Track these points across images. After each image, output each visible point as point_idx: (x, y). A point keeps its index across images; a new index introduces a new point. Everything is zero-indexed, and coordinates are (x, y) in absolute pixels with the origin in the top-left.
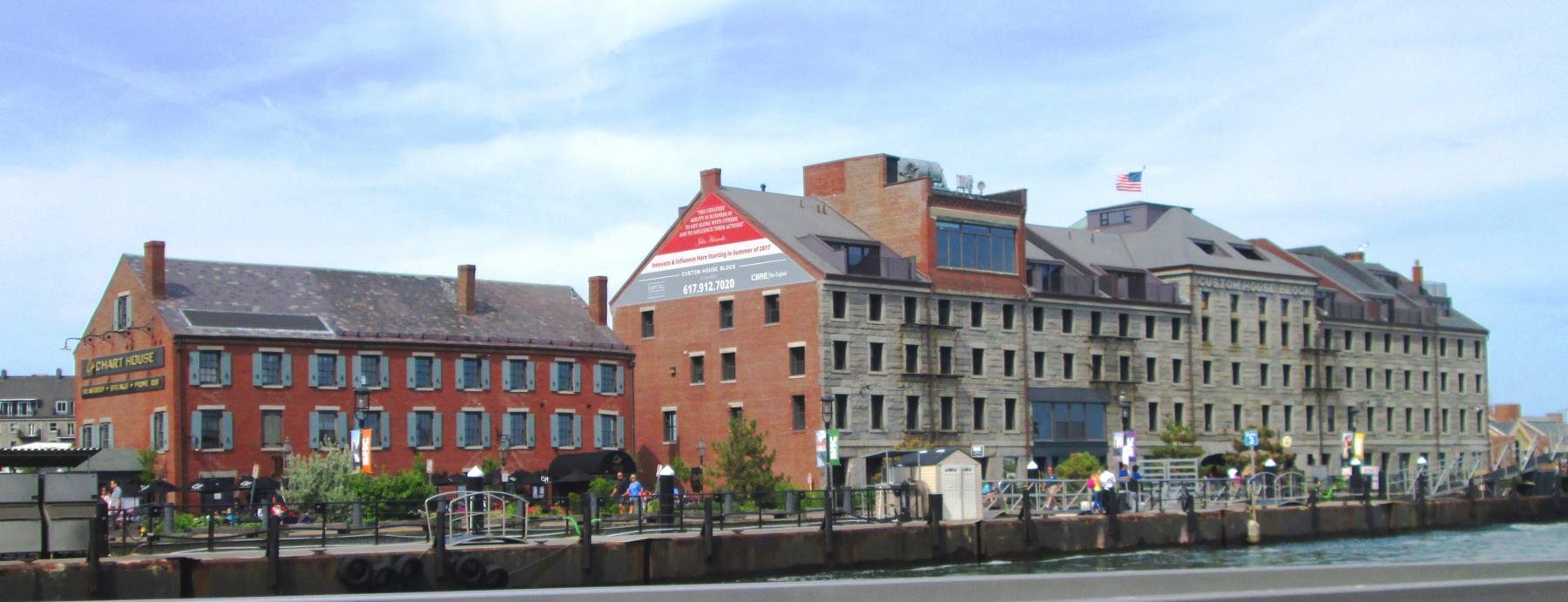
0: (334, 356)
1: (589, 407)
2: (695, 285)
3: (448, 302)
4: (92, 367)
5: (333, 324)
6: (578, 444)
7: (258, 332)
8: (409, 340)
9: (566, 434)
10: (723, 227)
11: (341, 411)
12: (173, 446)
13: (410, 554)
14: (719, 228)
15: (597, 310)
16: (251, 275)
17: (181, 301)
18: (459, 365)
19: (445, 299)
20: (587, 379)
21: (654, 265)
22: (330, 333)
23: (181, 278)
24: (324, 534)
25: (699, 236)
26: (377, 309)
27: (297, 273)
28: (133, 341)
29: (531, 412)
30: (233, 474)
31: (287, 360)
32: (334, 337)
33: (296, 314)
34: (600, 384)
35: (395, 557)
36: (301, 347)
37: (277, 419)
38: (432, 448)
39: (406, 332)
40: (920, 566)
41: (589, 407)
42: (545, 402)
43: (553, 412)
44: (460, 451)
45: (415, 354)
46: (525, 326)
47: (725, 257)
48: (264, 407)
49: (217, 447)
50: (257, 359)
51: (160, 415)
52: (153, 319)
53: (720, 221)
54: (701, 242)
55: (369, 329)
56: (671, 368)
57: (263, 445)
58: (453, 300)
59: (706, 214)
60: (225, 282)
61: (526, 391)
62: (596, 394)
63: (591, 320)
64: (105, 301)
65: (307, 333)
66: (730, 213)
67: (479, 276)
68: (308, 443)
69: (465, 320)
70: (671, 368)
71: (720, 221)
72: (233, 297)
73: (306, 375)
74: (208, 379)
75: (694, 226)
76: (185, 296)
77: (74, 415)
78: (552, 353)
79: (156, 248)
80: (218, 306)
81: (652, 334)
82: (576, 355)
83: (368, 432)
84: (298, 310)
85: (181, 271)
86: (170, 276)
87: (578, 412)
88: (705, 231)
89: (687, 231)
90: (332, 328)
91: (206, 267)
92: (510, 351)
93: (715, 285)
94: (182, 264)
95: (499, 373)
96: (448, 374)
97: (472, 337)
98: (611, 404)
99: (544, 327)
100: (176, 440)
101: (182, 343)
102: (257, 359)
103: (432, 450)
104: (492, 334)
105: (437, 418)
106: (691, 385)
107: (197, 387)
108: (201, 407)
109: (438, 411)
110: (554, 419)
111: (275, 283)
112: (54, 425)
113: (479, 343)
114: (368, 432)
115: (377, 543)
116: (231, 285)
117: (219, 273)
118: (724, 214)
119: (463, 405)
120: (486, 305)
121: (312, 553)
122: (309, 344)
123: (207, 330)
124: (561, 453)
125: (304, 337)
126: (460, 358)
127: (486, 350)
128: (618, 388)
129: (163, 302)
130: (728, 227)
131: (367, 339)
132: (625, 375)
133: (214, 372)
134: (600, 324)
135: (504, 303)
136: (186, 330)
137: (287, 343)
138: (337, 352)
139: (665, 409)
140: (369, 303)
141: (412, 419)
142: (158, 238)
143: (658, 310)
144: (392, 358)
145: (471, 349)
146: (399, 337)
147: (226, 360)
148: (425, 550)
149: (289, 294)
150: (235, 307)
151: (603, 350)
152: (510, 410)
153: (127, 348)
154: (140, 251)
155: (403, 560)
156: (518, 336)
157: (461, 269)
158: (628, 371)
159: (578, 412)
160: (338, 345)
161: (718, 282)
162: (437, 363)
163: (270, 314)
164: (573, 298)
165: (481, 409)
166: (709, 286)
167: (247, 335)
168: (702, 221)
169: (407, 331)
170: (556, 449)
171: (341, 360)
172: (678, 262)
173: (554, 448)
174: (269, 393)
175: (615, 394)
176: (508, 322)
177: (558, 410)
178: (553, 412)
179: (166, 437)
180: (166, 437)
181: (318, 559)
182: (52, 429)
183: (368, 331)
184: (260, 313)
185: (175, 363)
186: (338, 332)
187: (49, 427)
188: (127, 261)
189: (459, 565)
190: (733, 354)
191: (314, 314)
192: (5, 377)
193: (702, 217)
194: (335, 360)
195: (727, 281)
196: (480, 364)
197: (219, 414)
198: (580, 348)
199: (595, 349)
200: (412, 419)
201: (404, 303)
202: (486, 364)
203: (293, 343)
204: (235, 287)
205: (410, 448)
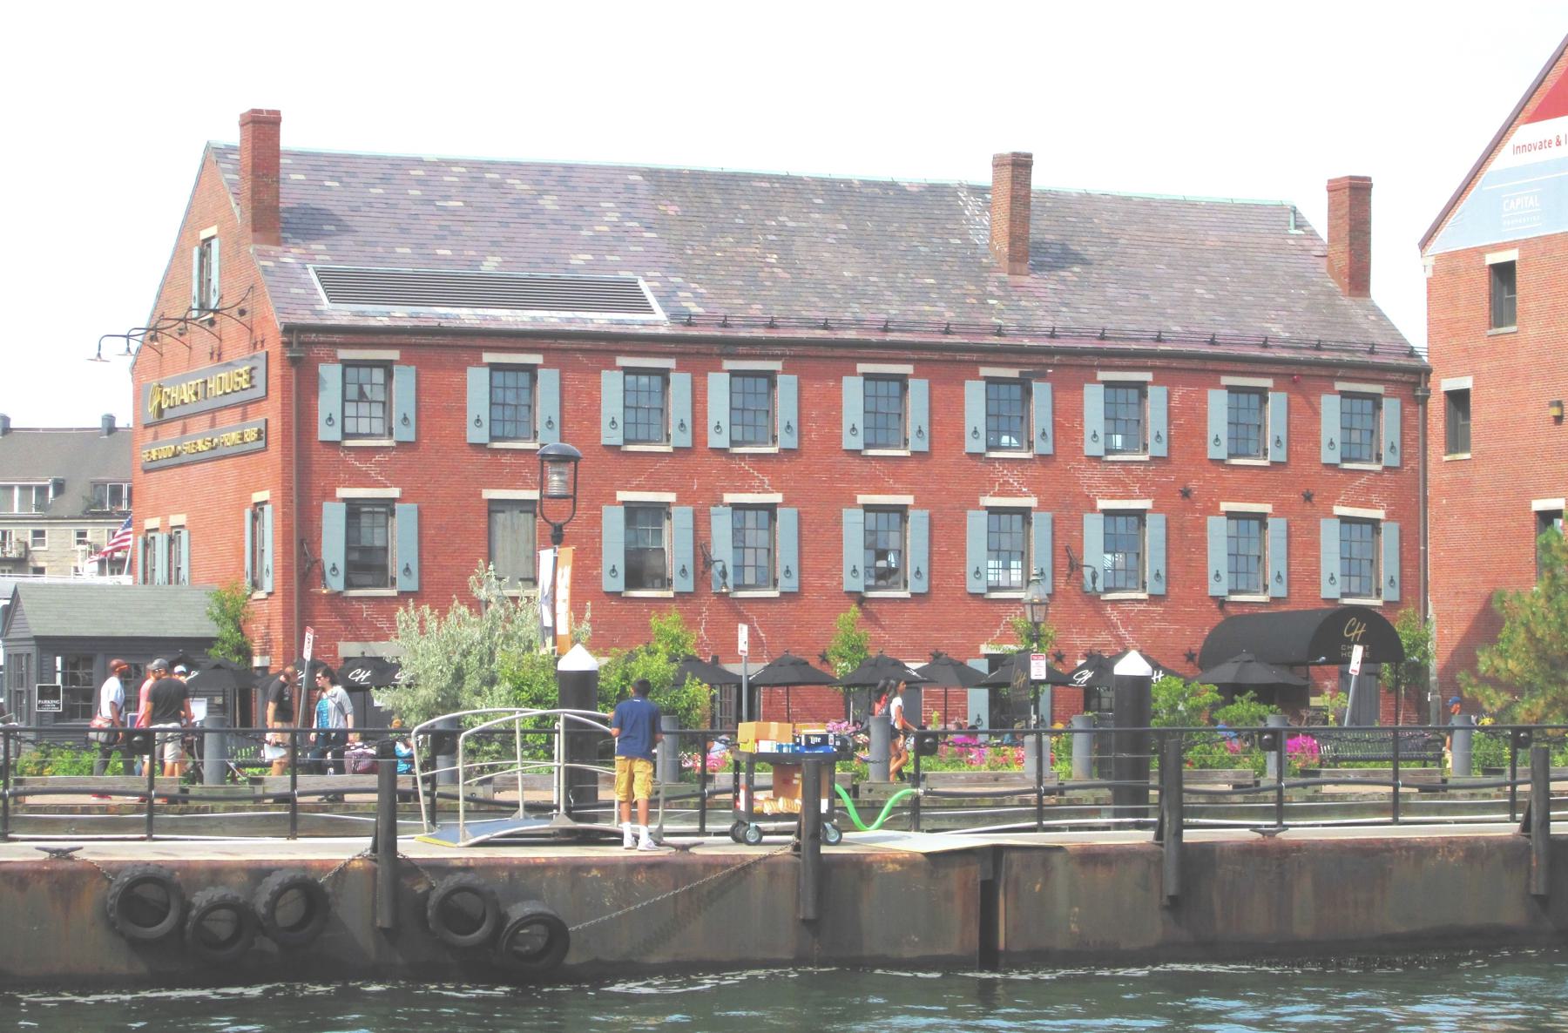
0: (664, 374)
1: (1308, 498)
3: (968, 243)
4: (156, 403)
5: (666, 298)
6: (1280, 590)
7: (484, 318)
8: (850, 335)
9: (1246, 564)
11: (1038, 509)
12: (280, 582)
13: (135, 864)
15: (1343, 261)
16: (495, 185)
17: (316, 246)
18: (974, 395)
19: (963, 235)
20: (1302, 432)
21: (1518, 149)
22: (657, 320)
23: (332, 195)
24: (1396, 794)
26: (787, 262)
27: (609, 180)
29: (1157, 509)
31: (787, 385)
33: (584, 275)
35: (259, 872)
37: (525, 520)
38: (905, 594)
39: (848, 316)
40: (899, 970)
41: (1308, 498)
42: (1193, 485)
43: (1214, 510)
44: (974, 604)
45: (862, 368)
46: (1154, 300)
49: (385, 586)
50: (477, 381)
55: (756, 309)
56: (1552, 404)
58: (981, 239)
60: (431, 202)
61: (1145, 458)
62: (1327, 466)
63: (1332, 285)
64: (180, 252)
65: (599, 320)
67: (1040, 180)
68: (598, 578)
69: (1003, 284)
70: (1552, 404)
73: (596, 422)
74: (364, 429)
76: (329, 234)
77: (124, 508)
78: (1210, 365)
79: (263, 126)
80: (403, 258)
81: (1512, 321)
82: (1274, 369)
83: (567, 553)
84: (589, 266)
85: (332, 178)
86: (294, 186)
87: (1278, 512)
90: (665, 308)
91: (392, 170)
92: (1106, 361)
95: (1079, 413)
96: (945, 415)
97: (1012, 325)
98: (1368, 490)
99: (1201, 299)
100: (286, 570)
101: (301, 344)
102: (477, 381)
104: (1065, 319)
105: (918, 521)
107: (334, 445)
108: (343, 492)
110: (1217, 528)
111: (549, 203)
112: (82, 534)
113: (1027, 342)
114: (567, 553)
115: (293, 834)
116: (444, 209)
117: (420, 182)
119: (985, 493)
120: (1064, 247)
121: (44, 856)
122: (603, 345)
123: (363, 314)
124: (1232, 610)
125: (591, 327)
126: (976, 377)
127: (1044, 360)
128: (1384, 452)
129: (274, 250)
131: (744, 333)
132: (1403, 419)
133: (378, 410)
135: (1114, 243)
136: (316, 313)
137: (546, 343)
138: (669, 363)
139: (1539, 505)
140: (769, 247)
141: (853, 523)
142: (265, 105)
143: (1524, 259)
144: (421, 365)
146: (826, 327)
147: (405, 379)
148: (347, 857)
149: (577, 228)
150: (445, 259)
151: (1346, 357)
152: (1102, 504)
154: (232, 135)
155: (273, 882)
156: (1131, 324)
157: (998, 163)
158: (1409, 409)
159: (1278, 512)
160: (672, 347)
162: (918, 390)
163: (525, 274)
164: (1293, 231)
165: (1031, 502)
167: (455, 324)
169: (855, 310)
170: (1221, 602)
171: (680, 383)
173: (1215, 598)
174: (506, 459)
175: (1377, 467)
176: (1112, 291)
177: (1225, 506)
178: (1214, 510)
179: (268, 560)
180: (268, 560)
181: (50, 873)
182: (79, 542)
183: (752, 312)
184: (504, 272)
185: (285, 389)
186: (674, 316)
187: (74, 538)
188: (215, 155)
189: (434, 898)
191: (625, 275)
192: (7, 430)
194: (666, 382)
196: (1028, 392)
197: (659, 512)
198: (1286, 354)
199: (1325, 356)
200: (853, 523)
201: (857, 246)
202: (1041, 392)
203: (565, 344)
204: (453, 212)
205: (850, 593)
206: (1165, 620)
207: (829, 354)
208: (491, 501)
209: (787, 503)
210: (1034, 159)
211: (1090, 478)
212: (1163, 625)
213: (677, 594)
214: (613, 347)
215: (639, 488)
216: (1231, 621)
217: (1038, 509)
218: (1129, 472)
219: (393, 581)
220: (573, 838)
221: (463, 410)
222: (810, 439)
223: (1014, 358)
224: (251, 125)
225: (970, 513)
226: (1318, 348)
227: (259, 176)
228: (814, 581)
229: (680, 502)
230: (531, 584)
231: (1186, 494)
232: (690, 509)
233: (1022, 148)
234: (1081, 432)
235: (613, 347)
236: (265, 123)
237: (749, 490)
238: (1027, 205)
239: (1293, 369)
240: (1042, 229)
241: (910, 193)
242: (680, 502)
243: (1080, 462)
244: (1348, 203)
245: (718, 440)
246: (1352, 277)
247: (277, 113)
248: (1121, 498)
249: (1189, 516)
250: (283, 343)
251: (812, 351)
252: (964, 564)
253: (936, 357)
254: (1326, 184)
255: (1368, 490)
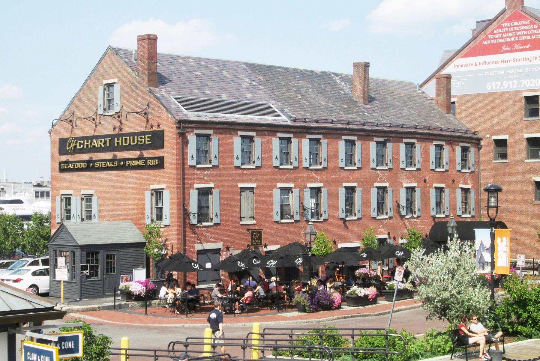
1: (453, 181)
2: (499, 83)
10: (529, 37)
11: (389, 187)
14: (523, 38)
21: (456, 66)
22: (283, 119)
25: (503, 44)
28: (121, 123)
30: (219, 245)
32: (289, 123)
34: (240, 157)
36: (267, 131)
41: (453, 181)
42: (427, 178)
47: (531, 61)
48: (241, 185)
49: (208, 221)
51: (159, 193)
52: (148, 104)
53: (525, 33)
54: (504, 48)
57: (241, 218)
59: (511, 27)
61: (415, 169)
65: (269, 119)
66: (536, 26)
71: (525, 33)
72: (204, 86)
73: (271, 157)
75: (498, 36)
78: (339, 132)
82: (446, 139)
88: (509, 40)
89: (491, 39)
92: (406, 136)
93: (520, 83)
94: (173, 59)
101: (183, 127)
103: (355, 220)
106: (494, 161)
109: (359, 186)
118: (531, 27)
119: (375, 182)
124: (436, 220)
130: (533, 37)
134: (447, 113)
137: (258, 128)
143: (460, 102)
145: (379, 133)
153: (114, 129)
160: (293, 130)
161: (523, 81)
166: (513, 84)
168: (506, 32)
170: (434, 218)
171: (447, 148)
172: (481, 64)
180: (166, 211)
190: (506, 140)
191: (265, 102)
193: (507, 29)
195: (533, 80)
203: (262, 128)
206: (420, 224)
207: (336, 133)
208: (242, 188)
209: (324, 187)
210: (158, 37)
211: (402, 176)
212: (420, 226)
213: (214, 224)
214: (276, 129)
215: (284, 182)
216: (436, 224)
217: (389, 187)
218: (411, 173)
219: (212, 220)
220: (170, 329)
221: (232, 153)
222: (330, 163)
223: (383, 135)
224: (364, 67)
225: (372, 189)
226: (416, 128)
227: (150, 60)
228: (332, 215)
229: (295, 187)
230: (252, 219)
231: (425, 181)
232: (298, 189)
233: (367, 61)
234: (399, 160)
235: (276, 129)
236: (152, 39)
237: (314, 182)
238: (368, 80)
239: (450, 139)
240: (161, 69)
241: (318, 74)
242: (295, 187)
243: (399, 170)
244: (446, 83)
245: (306, 164)
246: (447, 107)
247: (156, 36)
248: (409, 183)
249: (426, 189)
250: (176, 127)
251: (331, 132)
252: (370, 207)
253: (363, 134)
254: (137, 37)
255: (467, 178)
